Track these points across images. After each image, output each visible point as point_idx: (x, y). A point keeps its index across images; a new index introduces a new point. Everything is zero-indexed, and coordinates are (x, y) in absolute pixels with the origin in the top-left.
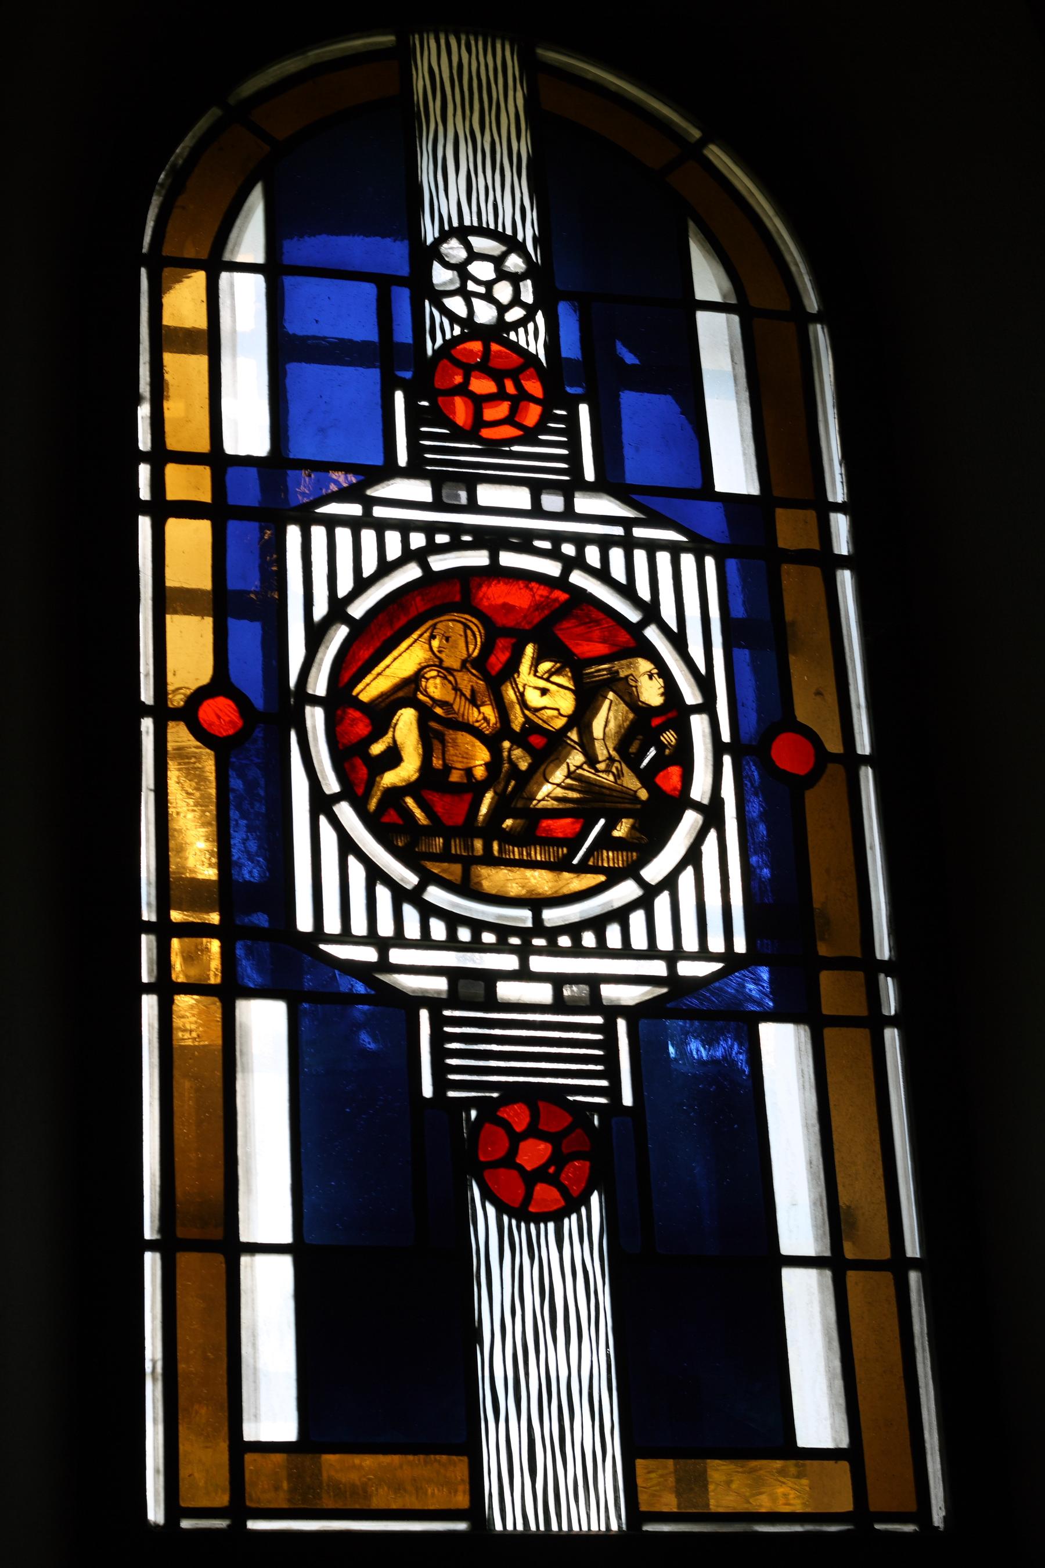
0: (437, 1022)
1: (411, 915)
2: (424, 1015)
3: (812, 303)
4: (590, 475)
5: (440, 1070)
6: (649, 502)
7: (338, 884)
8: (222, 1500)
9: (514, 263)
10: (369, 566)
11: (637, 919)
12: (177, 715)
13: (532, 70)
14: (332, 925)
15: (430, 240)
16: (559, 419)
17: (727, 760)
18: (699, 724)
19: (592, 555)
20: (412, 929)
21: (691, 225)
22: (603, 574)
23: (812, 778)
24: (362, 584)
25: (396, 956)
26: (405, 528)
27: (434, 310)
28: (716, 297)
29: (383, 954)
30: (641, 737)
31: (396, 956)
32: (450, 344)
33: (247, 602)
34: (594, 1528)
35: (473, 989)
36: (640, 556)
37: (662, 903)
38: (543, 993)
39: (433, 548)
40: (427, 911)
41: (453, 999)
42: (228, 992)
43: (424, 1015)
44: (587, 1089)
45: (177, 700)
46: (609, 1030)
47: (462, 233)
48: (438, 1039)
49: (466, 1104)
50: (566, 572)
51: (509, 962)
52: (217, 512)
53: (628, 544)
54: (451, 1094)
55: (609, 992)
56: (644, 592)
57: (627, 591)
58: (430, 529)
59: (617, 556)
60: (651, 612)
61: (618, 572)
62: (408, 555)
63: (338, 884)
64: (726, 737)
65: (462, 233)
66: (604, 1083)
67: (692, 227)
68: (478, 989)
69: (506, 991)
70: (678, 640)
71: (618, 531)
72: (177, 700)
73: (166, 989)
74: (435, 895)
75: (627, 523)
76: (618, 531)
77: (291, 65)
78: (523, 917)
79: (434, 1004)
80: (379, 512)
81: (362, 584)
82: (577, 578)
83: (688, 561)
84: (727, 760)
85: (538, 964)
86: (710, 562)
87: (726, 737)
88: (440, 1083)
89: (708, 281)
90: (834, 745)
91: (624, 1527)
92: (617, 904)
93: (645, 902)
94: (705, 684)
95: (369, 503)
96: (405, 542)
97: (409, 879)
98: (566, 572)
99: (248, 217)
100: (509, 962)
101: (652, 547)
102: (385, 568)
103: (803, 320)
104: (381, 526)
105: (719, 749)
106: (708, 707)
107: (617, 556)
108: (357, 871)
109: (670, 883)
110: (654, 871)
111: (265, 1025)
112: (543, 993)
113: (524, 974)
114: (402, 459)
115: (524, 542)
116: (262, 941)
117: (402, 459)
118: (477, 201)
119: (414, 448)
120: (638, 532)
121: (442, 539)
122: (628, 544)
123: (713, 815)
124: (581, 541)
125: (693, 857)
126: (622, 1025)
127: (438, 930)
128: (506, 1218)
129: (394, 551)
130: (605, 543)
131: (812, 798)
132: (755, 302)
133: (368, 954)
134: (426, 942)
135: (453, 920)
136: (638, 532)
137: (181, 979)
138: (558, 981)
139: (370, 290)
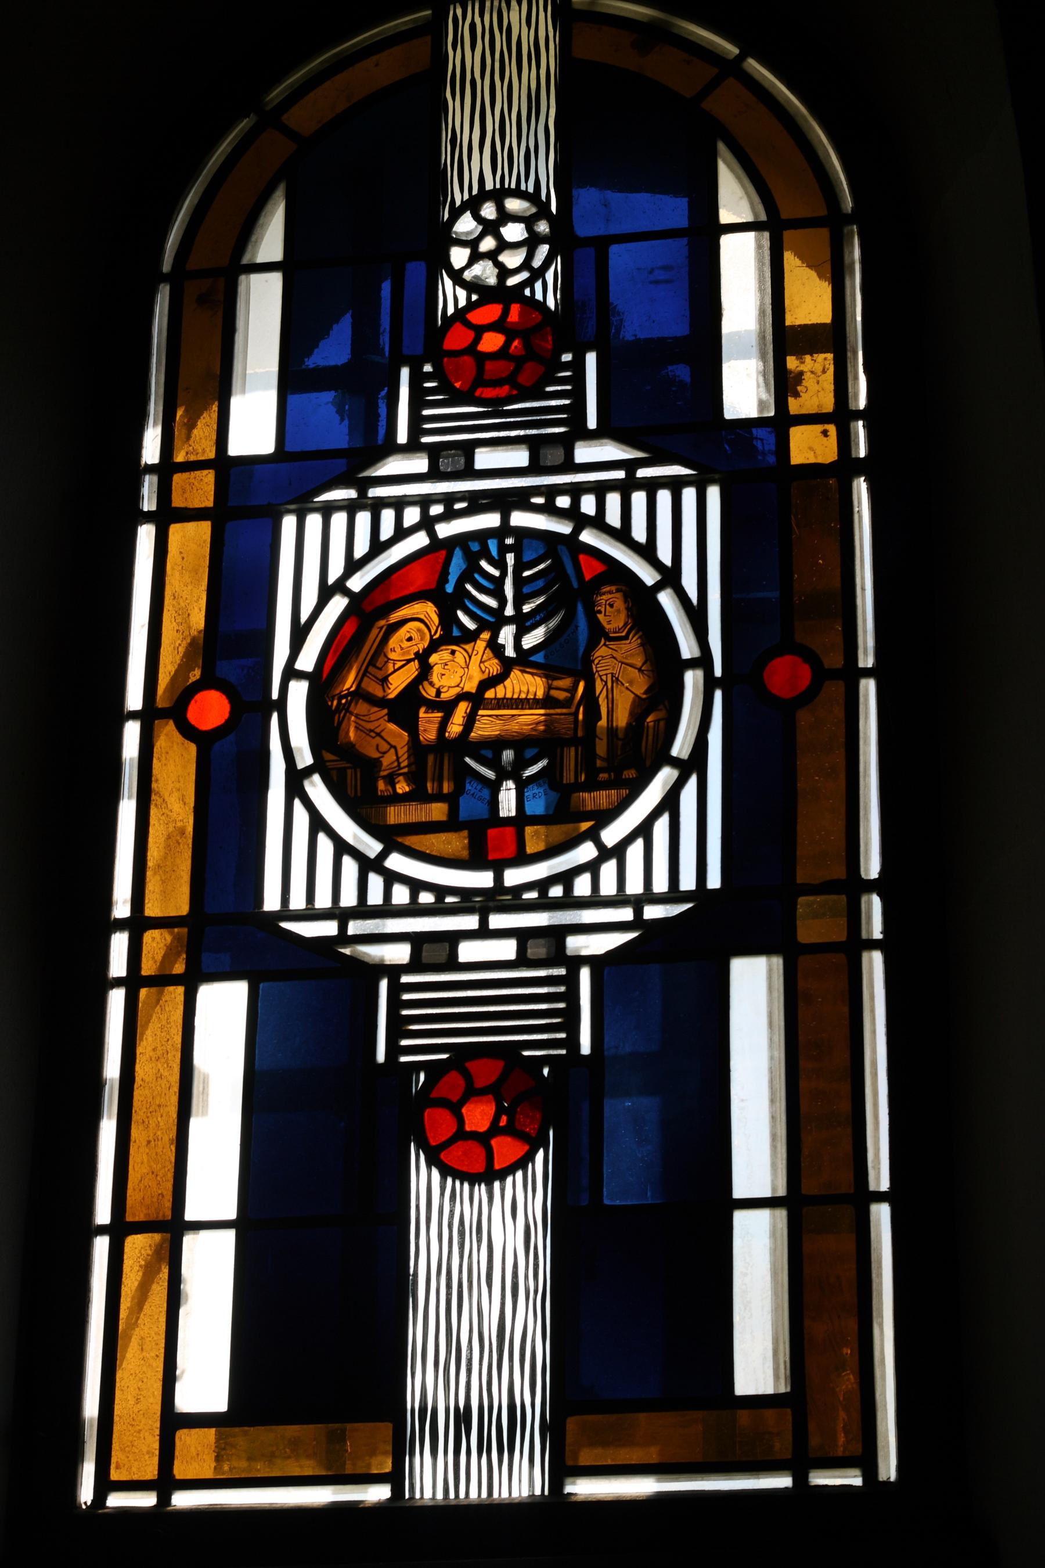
0: (396, 988)
1: (376, 883)
4: (592, 423)
7: (307, 861)
8: (151, 1472)
10: (361, 548)
16: (566, 366)
17: (718, 695)
20: (375, 898)
21: (721, 147)
22: (623, 535)
23: (808, 697)
24: (353, 566)
30: (549, 329)
31: (354, 928)
32: (460, 314)
33: (240, 590)
34: (515, 1494)
35: (434, 951)
36: (639, 499)
38: (507, 950)
40: (391, 878)
41: (415, 965)
43: (384, 985)
44: (537, 1043)
46: (572, 981)
48: (395, 1004)
49: (418, 1066)
51: (471, 922)
53: (626, 488)
54: (403, 1059)
55: (575, 944)
56: (665, 555)
57: (647, 551)
60: (671, 577)
62: (401, 533)
63: (307, 861)
67: (721, 147)
68: (440, 953)
69: (469, 951)
74: (396, 862)
75: (629, 466)
79: (394, 971)
81: (353, 566)
85: (497, 921)
90: (834, 660)
91: (546, 1493)
92: (358, 575)
93: (593, 867)
97: (372, 847)
100: (471, 922)
101: (652, 487)
102: (378, 547)
104: (376, 507)
108: (325, 846)
109: (619, 852)
111: (223, 1008)
112: (507, 950)
113: (484, 933)
116: (226, 928)
121: (436, 510)
122: (626, 488)
126: (585, 974)
127: (401, 895)
128: (449, 1180)
129: (387, 531)
130: (600, 490)
131: (804, 718)
133: (329, 928)
134: (387, 910)
135: (416, 886)
136: (642, 473)
138: (522, 935)
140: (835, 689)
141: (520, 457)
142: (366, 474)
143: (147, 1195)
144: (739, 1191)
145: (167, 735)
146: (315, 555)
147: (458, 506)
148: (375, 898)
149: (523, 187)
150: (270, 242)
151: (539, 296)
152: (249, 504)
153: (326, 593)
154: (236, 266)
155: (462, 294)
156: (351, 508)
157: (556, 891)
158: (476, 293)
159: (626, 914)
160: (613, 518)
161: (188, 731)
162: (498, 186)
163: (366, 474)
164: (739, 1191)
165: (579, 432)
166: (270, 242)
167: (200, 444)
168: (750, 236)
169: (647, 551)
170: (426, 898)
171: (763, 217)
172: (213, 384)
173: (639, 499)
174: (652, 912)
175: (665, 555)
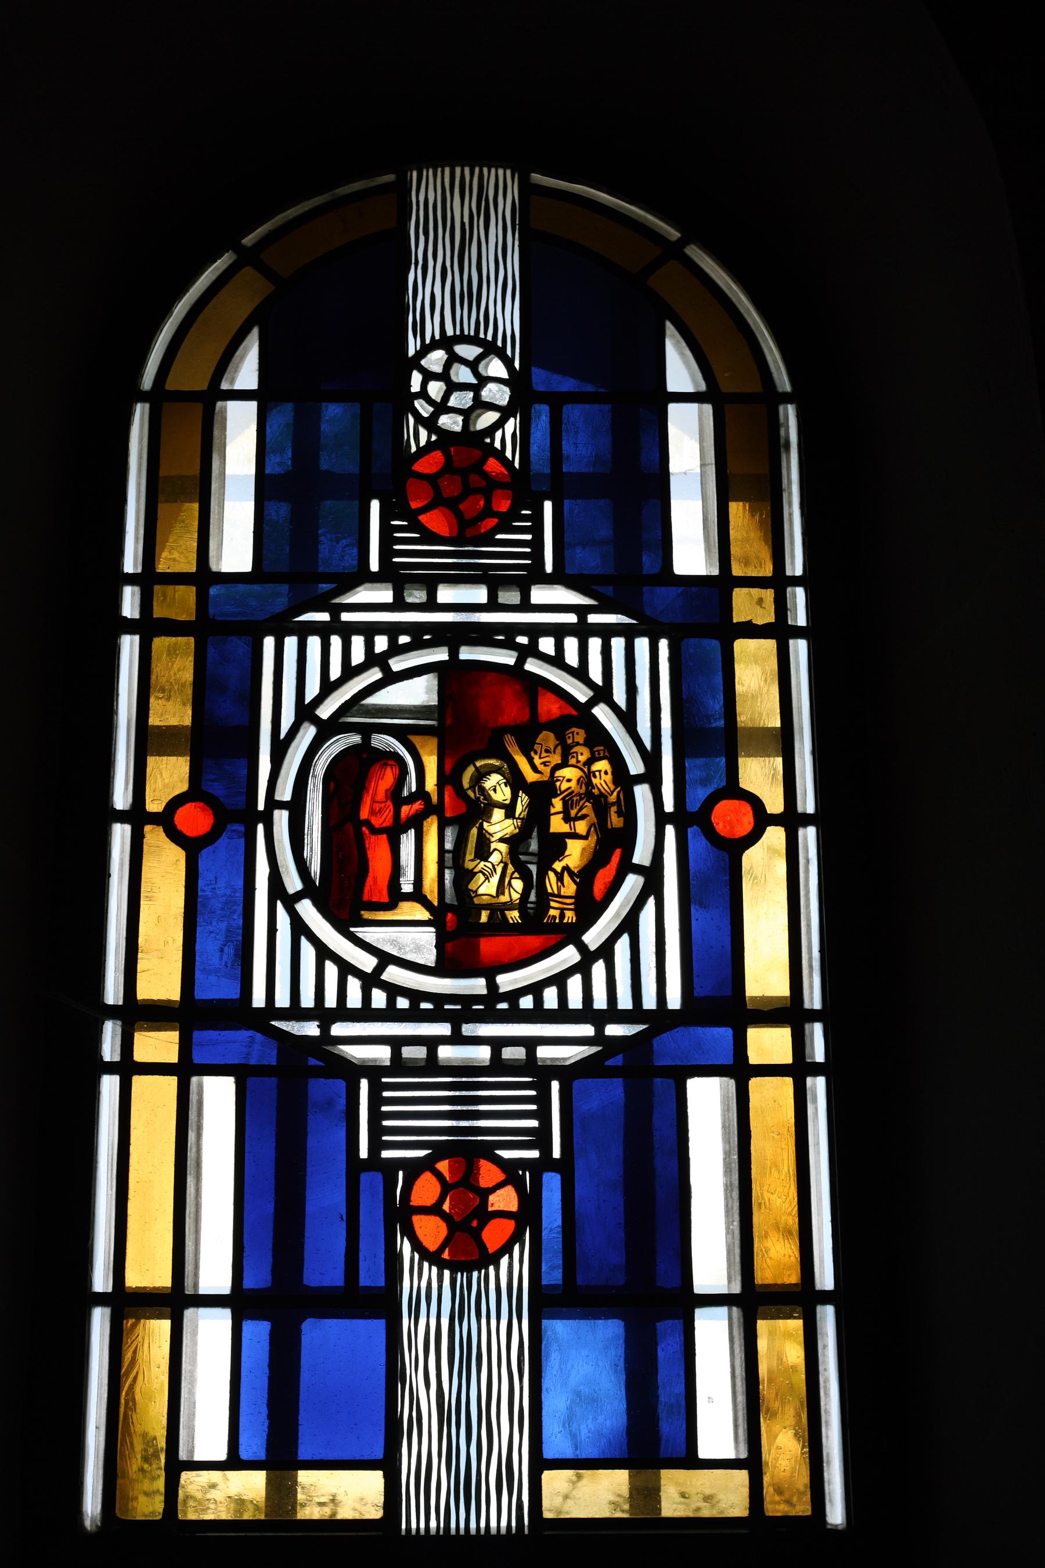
2: (364, 1084)
3: (784, 382)
5: (376, 1131)
6: (604, 590)
9: (496, 368)
11: (575, 984)
12: (155, 819)
13: (527, 189)
14: (283, 1000)
15: (411, 352)
17: (670, 831)
18: (642, 793)
19: (547, 645)
20: (354, 1000)
22: (557, 661)
24: (328, 687)
25: (338, 1029)
26: (369, 631)
27: (368, 934)
28: (689, 388)
29: (325, 1028)
31: (338, 1029)
33: (221, 738)
36: (595, 644)
37: (599, 969)
39: (395, 650)
40: (393, 991)
42: (185, 1070)
43: (364, 1084)
45: (154, 805)
47: (446, 343)
50: (521, 661)
52: (203, 629)
56: (596, 674)
57: (581, 673)
58: (392, 630)
59: (571, 644)
60: (603, 694)
61: (572, 658)
64: (669, 806)
65: (446, 343)
66: (529, 537)
70: (628, 718)
71: (571, 618)
72: (154, 805)
73: (128, 1068)
75: (581, 611)
76: (571, 618)
77: (291, 213)
78: (397, 664)
79: (373, 1072)
80: (346, 617)
81: (328, 687)
82: (532, 666)
83: (642, 645)
84: (670, 831)
86: (663, 645)
87: (669, 806)
88: (376, 1145)
89: (680, 371)
93: (583, 968)
94: (652, 759)
95: (336, 611)
96: (369, 645)
98: (521, 661)
99: (243, 357)
100: (443, 1029)
101: (606, 633)
102: (349, 672)
103: (774, 399)
104: (347, 631)
105: (661, 819)
106: (652, 777)
107: (571, 644)
108: (308, 953)
109: (606, 951)
110: (593, 938)
113: (457, 1039)
114: (374, 566)
115: (484, 635)
117: (374, 566)
118: (465, 304)
119: (386, 552)
120: (593, 618)
123: (653, 885)
124: (535, 631)
125: (629, 925)
127: (379, 999)
129: (358, 656)
130: (559, 632)
131: (753, 858)
132: (726, 386)
134: (366, 1014)
136: (593, 618)
137: (541, 388)
139: (547, 1476)
140: (775, 836)
141: (479, 594)
142: (337, 601)
143: (190, 378)
144: (252, 406)
145: (154, 836)
146: (291, 671)
147: (425, 1006)
148: (354, 1000)
149: (482, 336)
150: (535, 834)
151: (497, 444)
152: (226, 628)
153: (305, 712)
154: (213, 396)
155: (423, 434)
156: (324, 631)
157: (527, 1002)
158: (436, 434)
159: (587, 1030)
160: (572, 658)
161: (175, 836)
162: (458, 333)
163: (337, 601)
164: (252, 406)
165: (537, 576)
166: (246, 374)
167: (178, 557)
168: (693, 407)
169: (581, 673)
170: (403, 1003)
171: (703, 387)
172: (190, 483)
173: (595, 644)
174: (613, 1030)
175: (596, 674)
